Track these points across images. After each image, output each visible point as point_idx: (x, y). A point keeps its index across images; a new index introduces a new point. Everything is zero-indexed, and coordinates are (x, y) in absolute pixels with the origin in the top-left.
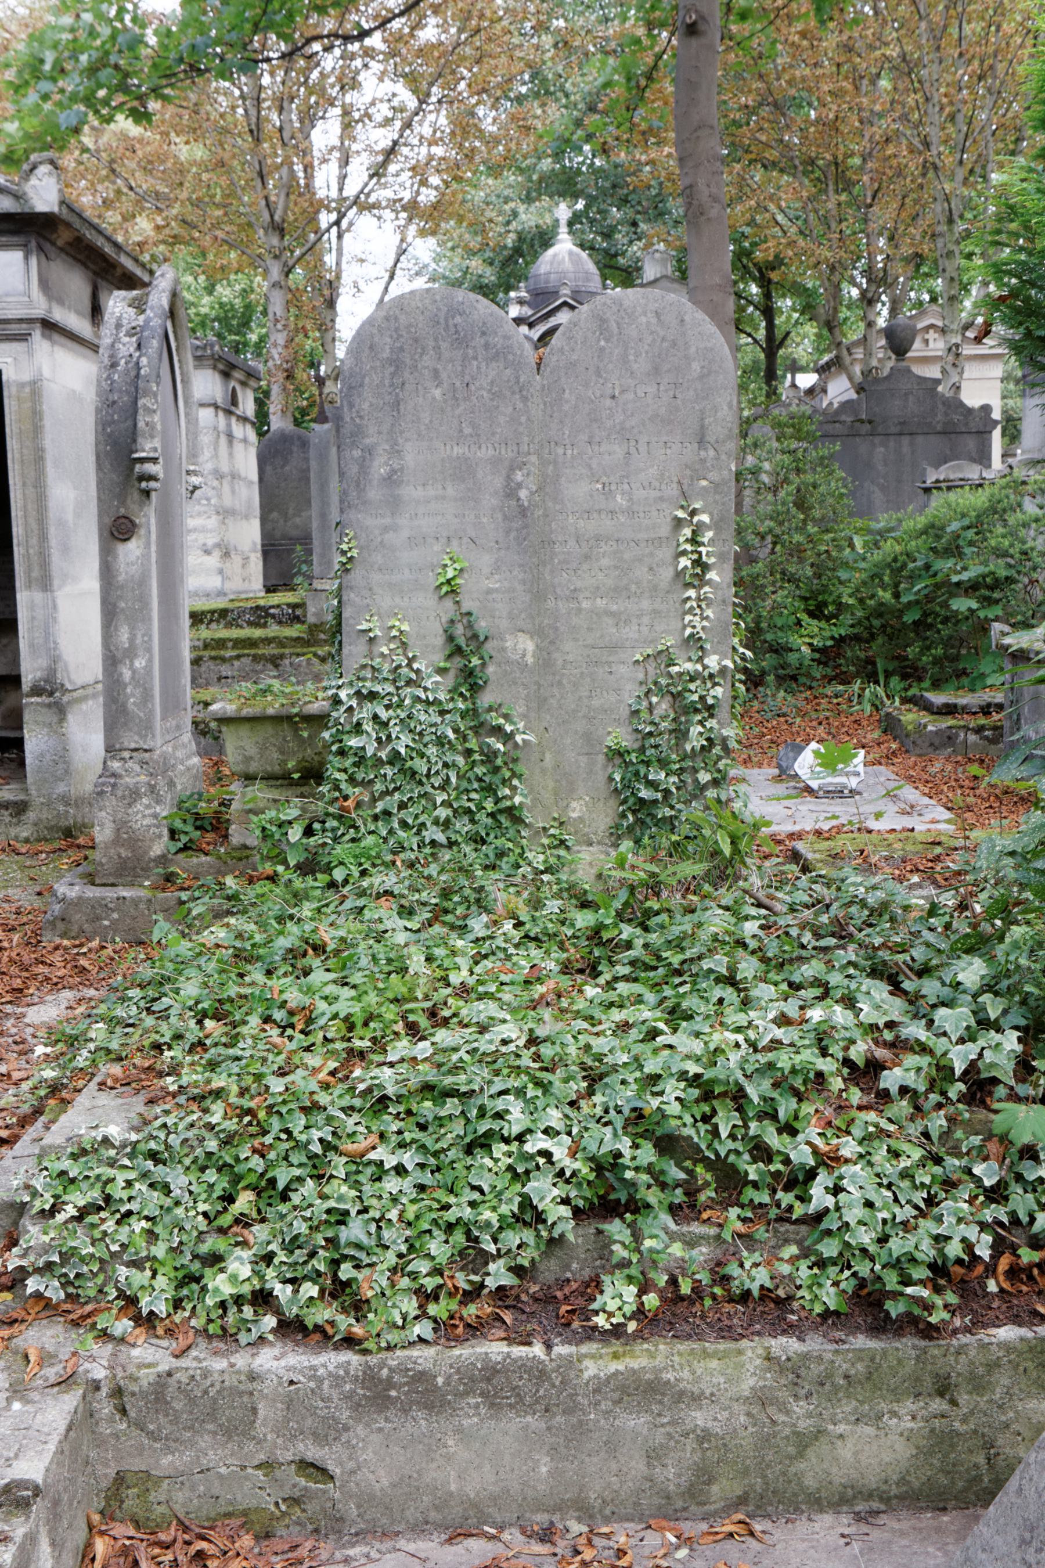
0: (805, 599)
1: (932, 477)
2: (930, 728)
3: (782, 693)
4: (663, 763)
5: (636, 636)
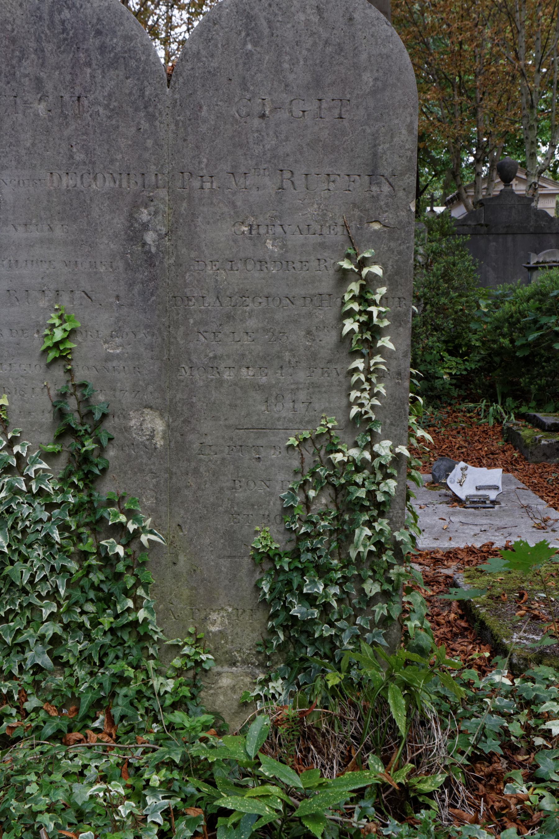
0: (445, 342)
1: (533, 261)
2: (543, 442)
3: (431, 409)
4: (323, 571)
5: (290, 415)
